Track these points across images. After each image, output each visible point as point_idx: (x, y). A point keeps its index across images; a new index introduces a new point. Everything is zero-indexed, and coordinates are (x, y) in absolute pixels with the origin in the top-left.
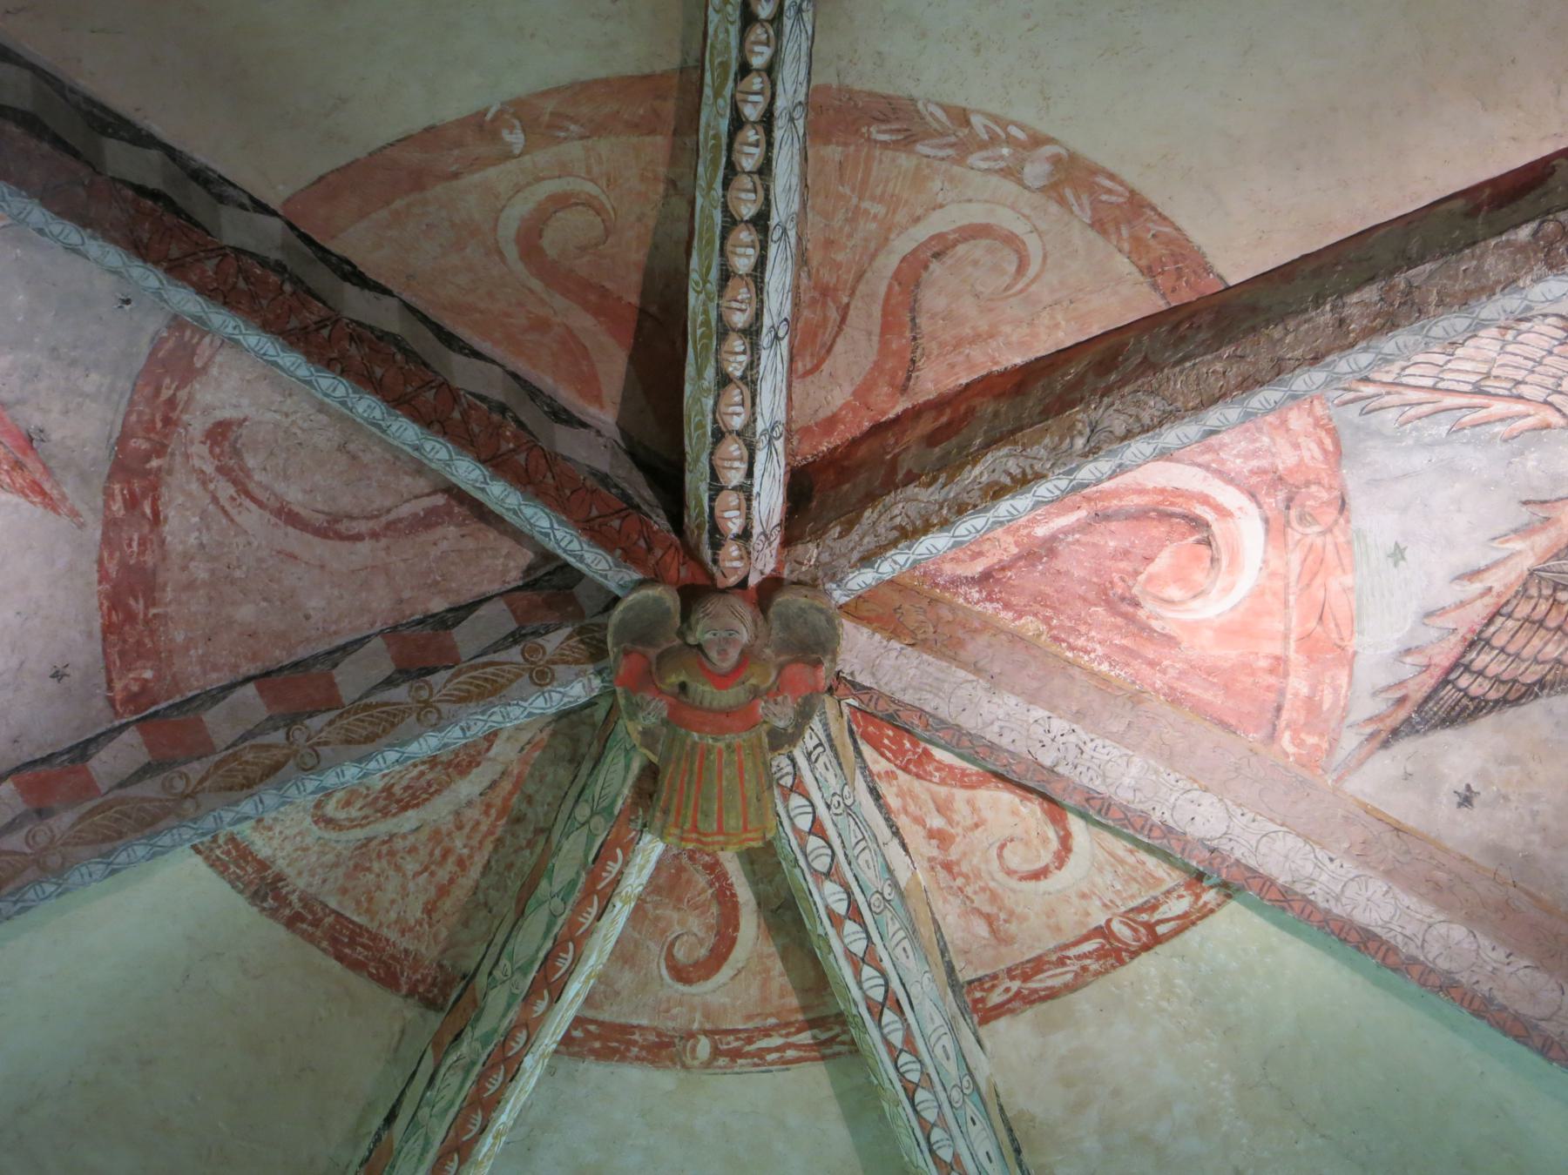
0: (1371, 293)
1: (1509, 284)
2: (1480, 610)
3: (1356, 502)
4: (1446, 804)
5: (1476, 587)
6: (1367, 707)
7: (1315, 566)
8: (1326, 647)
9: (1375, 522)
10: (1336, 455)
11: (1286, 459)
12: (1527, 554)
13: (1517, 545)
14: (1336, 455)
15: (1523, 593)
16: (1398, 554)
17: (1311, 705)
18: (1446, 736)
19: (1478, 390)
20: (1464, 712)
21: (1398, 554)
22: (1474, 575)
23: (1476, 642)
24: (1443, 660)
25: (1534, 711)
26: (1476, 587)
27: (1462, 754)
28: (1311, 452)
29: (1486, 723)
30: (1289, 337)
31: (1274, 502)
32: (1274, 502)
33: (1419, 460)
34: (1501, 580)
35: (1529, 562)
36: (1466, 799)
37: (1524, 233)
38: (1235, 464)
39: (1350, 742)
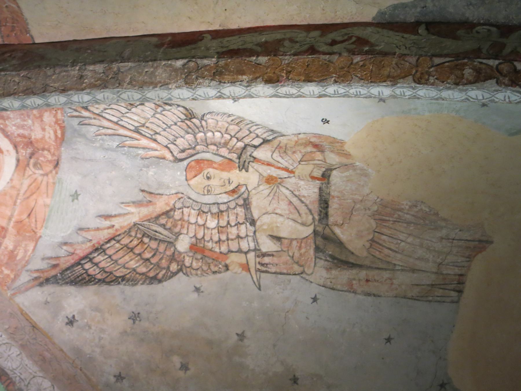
0: (99, 68)
1: (165, 85)
2: (105, 234)
3: (64, 165)
4: (60, 322)
5: (107, 223)
6: (38, 264)
7: (34, 190)
8: (27, 230)
9: (70, 177)
10: (61, 140)
11: (37, 134)
12: (136, 215)
13: (132, 209)
14: (61, 140)
15: (128, 233)
16: (75, 196)
17: (12, 255)
18: (71, 289)
19: (137, 131)
20: (83, 280)
21: (75, 196)
22: (107, 217)
23: (99, 249)
24: (81, 251)
25: (116, 289)
26: (107, 223)
27: (76, 300)
28: (50, 134)
29: (92, 288)
30: (55, 76)
31: (24, 153)
32: (24, 153)
33: (100, 155)
34: (120, 223)
35: (135, 219)
36: (71, 322)
37: (179, 63)
38: (12, 129)
39: (25, 278)
